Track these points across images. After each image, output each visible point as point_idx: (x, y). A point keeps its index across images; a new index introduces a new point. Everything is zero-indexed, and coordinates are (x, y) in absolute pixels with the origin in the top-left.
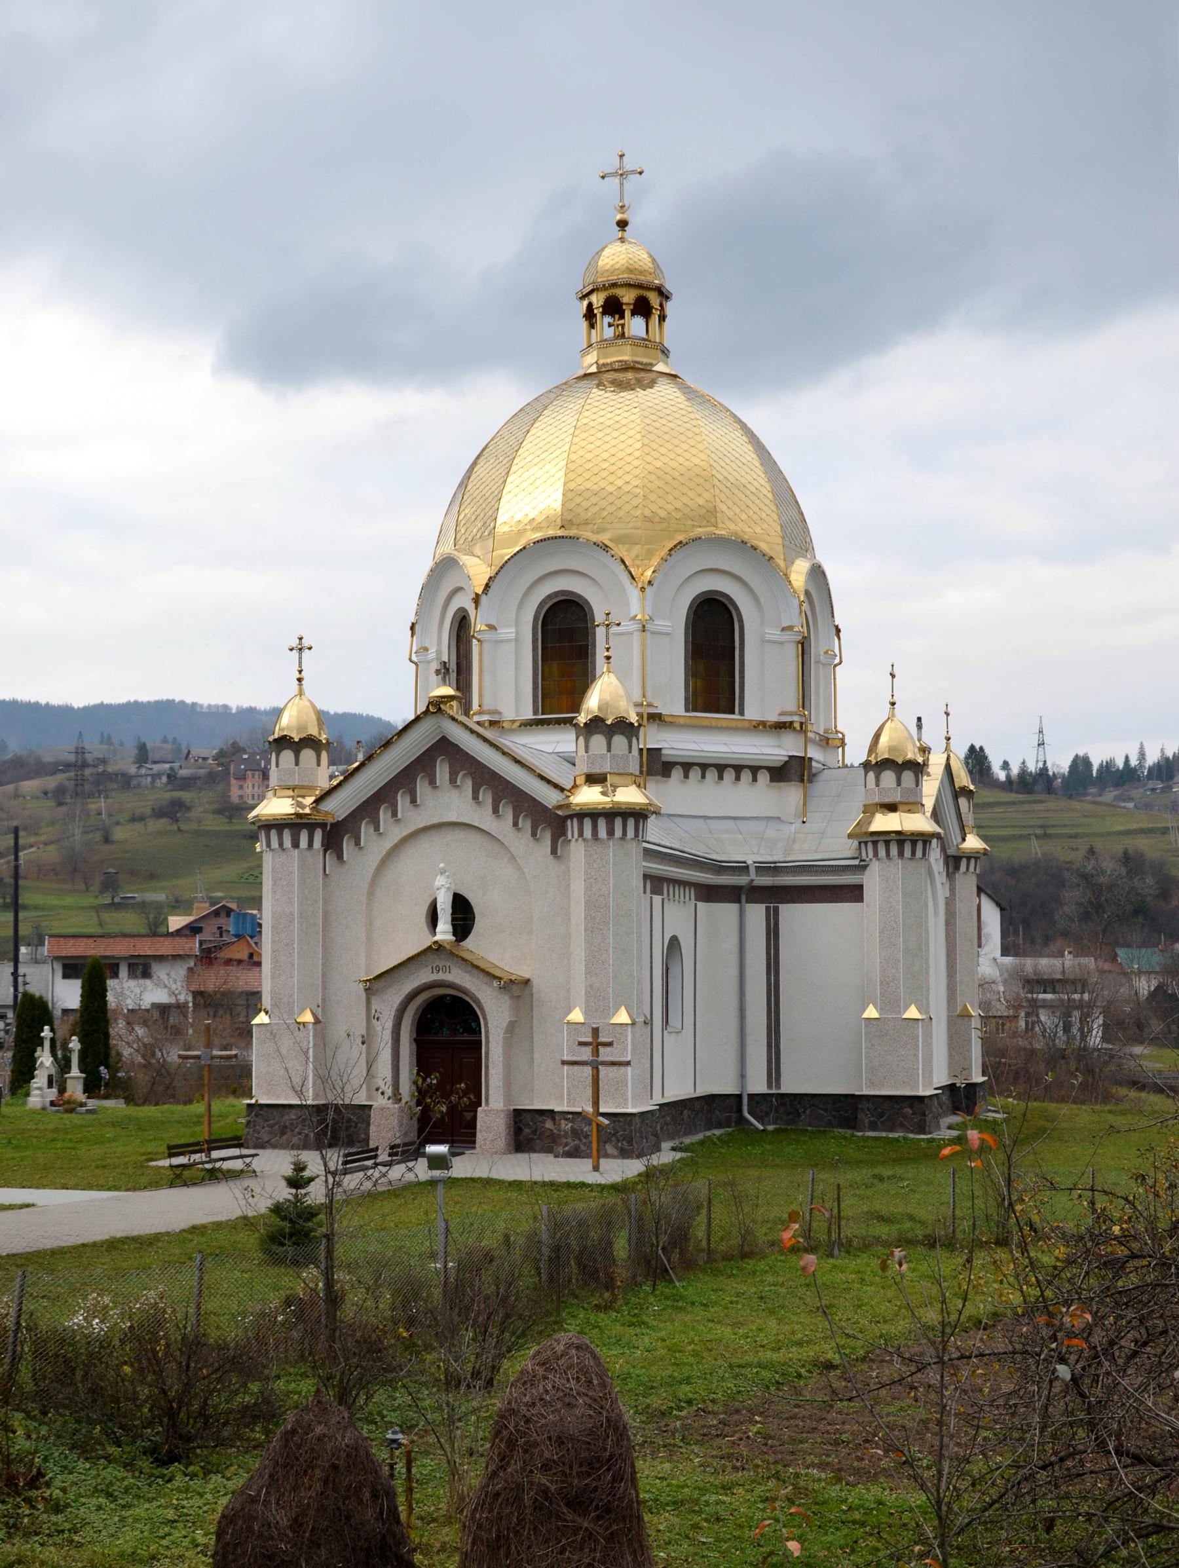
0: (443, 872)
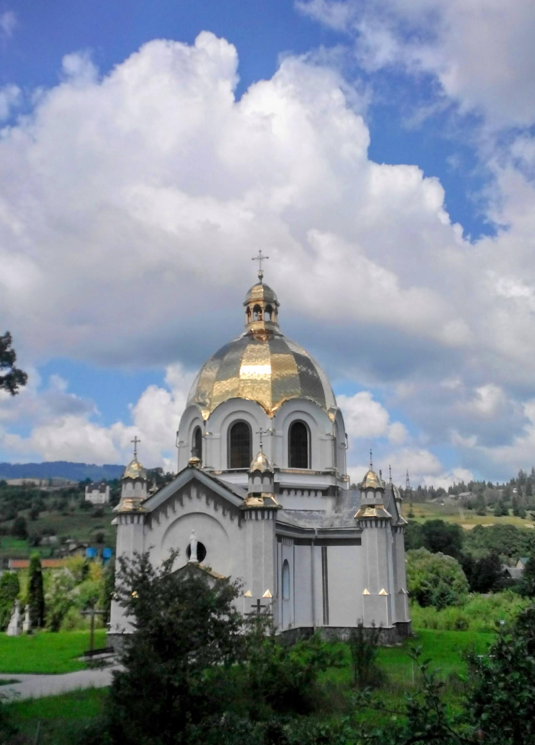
0: (193, 533)
